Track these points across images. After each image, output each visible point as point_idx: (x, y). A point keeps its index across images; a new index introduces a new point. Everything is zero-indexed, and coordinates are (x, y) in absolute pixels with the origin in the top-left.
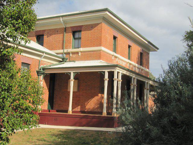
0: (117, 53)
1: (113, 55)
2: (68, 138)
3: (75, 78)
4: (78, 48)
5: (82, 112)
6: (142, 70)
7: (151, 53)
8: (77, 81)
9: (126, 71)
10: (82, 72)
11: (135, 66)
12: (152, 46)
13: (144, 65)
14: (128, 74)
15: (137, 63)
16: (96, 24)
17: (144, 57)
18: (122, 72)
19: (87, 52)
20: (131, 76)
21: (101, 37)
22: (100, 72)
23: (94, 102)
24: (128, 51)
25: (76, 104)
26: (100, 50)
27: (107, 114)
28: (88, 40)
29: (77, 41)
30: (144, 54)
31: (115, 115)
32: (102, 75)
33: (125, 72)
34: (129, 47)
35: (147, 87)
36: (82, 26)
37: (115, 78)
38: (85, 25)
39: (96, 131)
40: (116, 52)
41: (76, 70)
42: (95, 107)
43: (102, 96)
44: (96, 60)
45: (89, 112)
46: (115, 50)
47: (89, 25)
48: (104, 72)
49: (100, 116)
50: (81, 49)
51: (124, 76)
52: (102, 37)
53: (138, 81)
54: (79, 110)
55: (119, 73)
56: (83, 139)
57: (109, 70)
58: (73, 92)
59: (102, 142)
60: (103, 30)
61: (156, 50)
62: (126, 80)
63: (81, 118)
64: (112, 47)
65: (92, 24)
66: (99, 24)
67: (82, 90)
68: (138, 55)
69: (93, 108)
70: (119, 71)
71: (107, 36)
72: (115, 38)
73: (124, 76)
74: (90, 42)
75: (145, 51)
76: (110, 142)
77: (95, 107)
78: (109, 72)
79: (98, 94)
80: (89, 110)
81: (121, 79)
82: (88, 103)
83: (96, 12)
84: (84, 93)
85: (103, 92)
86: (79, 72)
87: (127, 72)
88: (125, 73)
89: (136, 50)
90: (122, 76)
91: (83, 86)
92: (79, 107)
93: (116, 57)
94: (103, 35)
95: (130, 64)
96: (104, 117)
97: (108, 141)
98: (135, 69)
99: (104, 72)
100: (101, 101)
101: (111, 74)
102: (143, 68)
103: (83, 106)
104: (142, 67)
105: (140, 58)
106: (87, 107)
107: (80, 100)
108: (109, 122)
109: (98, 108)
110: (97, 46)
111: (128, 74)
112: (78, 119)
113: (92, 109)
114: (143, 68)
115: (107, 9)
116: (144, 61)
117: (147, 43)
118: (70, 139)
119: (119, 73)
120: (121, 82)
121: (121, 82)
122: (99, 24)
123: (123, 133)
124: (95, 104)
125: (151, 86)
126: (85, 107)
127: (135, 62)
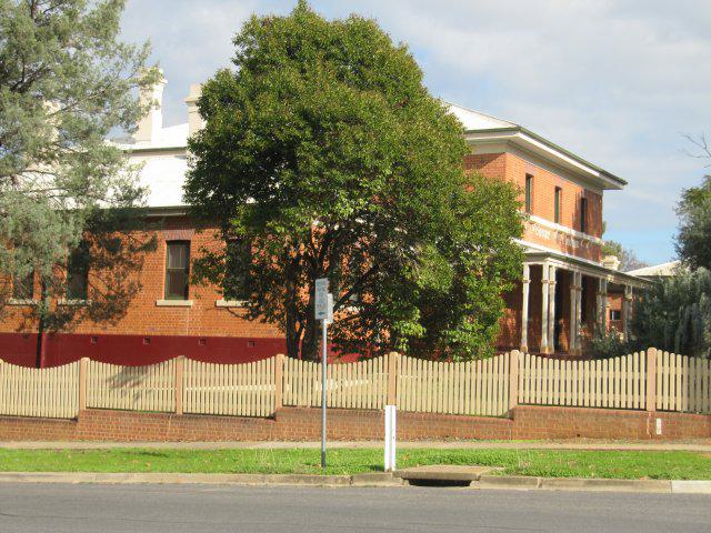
6: (586, 241)
7: (606, 194)
11: (569, 236)
15: (574, 227)
18: (556, 265)
20: (571, 269)
30: (590, 200)
33: (562, 265)
35: (602, 288)
53: (585, 279)
57: (531, 263)
61: (621, 186)
62: (563, 277)
66: (500, 154)
73: (561, 274)
75: (592, 192)
78: (531, 267)
88: (560, 266)
89: (572, 192)
95: (560, 233)
101: (536, 272)
102: (589, 238)
104: (585, 236)
111: (565, 267)
114: (589, 238)
116: (590, 219)
117: (597, 174)
122: (500, 154)
125: (610, 284)
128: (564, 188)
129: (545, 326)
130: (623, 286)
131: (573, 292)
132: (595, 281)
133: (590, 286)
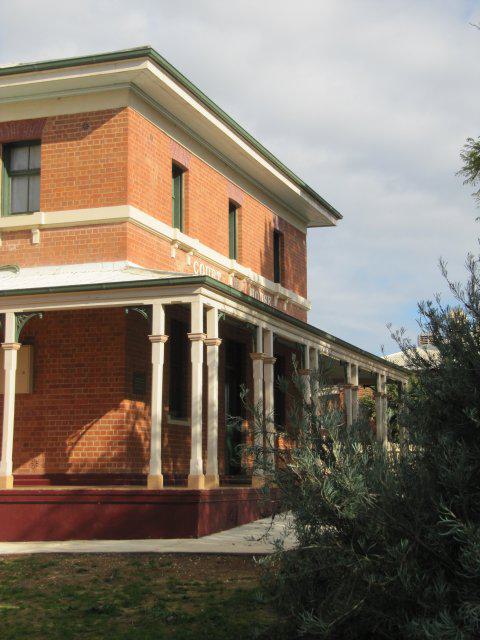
0: (187, 233)
1: (173, 242)
2: (14, 592)
3: (23, 338)
4: (29, 212)
5: (53, 478)
6: (282, 299)
7: (313, 235)
8: (28, 348)
9: (234, 304)
10: (62, 312)
11: (256, 286)
12: (315, 206)
13: (290, 281)
14: (240, 312)
15: (264, 273)
16: (103, 112)
17: (287, 249)
18: (221, 307)
19: (66, 228)
20: (255, 321)
21: (125, 168)
22: (130, 307)
23: (104, 433)
24: (228, 223)
25: (26, 445)
26: (123, 222)
27: (166, 483)
28: (72, 179)
29: (22, 183)
30: (288, 237)
31: (202, 486)
32: (139, 320)
33: (232, 308)
34: (233, 207)
35: (311, 364)
36: (42, 122)
37: (154, 333)
38: (53, 118)
39: (125, 555)
40: (184, 227)
41: (29, 304)
42: (109, 454)
43: (134, 406)
44: (107, 260)
45: (83, 476)
46: (179, 222)
47: (72, 116)
48: (149, 308)
49: (137, 492)
50: (44, 218)
51: (228, 324)
52: (131, 166)
53: (279, 342)
54: (40, 470)
55: (207, 313)
56: (82, 592)
57: (169, 301)
58: (18, 396)
59: (168, 600)
60: (131, 137)
61: (333, 220)
62: (236, 340)
63: (59, 503)
64: (170, 206)
65: (85, 114)
66: (107, 115)
67: (51, 387)
68: (266, 242)
69: (99, 460)
70: (212, 303)
71: (149, 161)
72: (178, 171)
73: (228, 324)
74: (81, 188)
75: (294, 218)
76: (201, 597)
77: (109, 454)
78: (167, 308)
79: (121, 400)
80: (84, 471)
81: (216, 336)
82: (79, 439)
83: (84, 64)
84: (58, 397)
85: (145, 394)
86: (43, 312)
87: (240, 307)
88: (230, 311)
89: (258, 219)
90: (221, 322)
91: (54, 371)
92: (41, 458)
93: (185, 249)
94: (132, 157)
95: (239, 277)
96: (156, 493)
97: (190, 593)
98: (258, 295)
99: (149, 308)
100: (133, 428)
101: (179, 319)
103: (57, 453)
104: (282, 290)
105: (272, 253)
106: (75, 456)
107: (43, 429)
108: (178, 511)
109: (119, 459)
110: (110, 202)
111: (241, 315)
112: (43, 508)
113: (96, 465)
115: (146, 48)
116: (289, 266)
118: (25, 598)
119: (207, 313)
120: (220, 347)
121: (217, 348)
123: (288, 561)
124: (110, 444)
125: (323, 359)
126: (66, 457)
127: (254, 270)
128: (243, 205)
129: (197, 429)
130: (344, 364)
131: (258, 365)
132: (299, 349)
133: (287, 357)
